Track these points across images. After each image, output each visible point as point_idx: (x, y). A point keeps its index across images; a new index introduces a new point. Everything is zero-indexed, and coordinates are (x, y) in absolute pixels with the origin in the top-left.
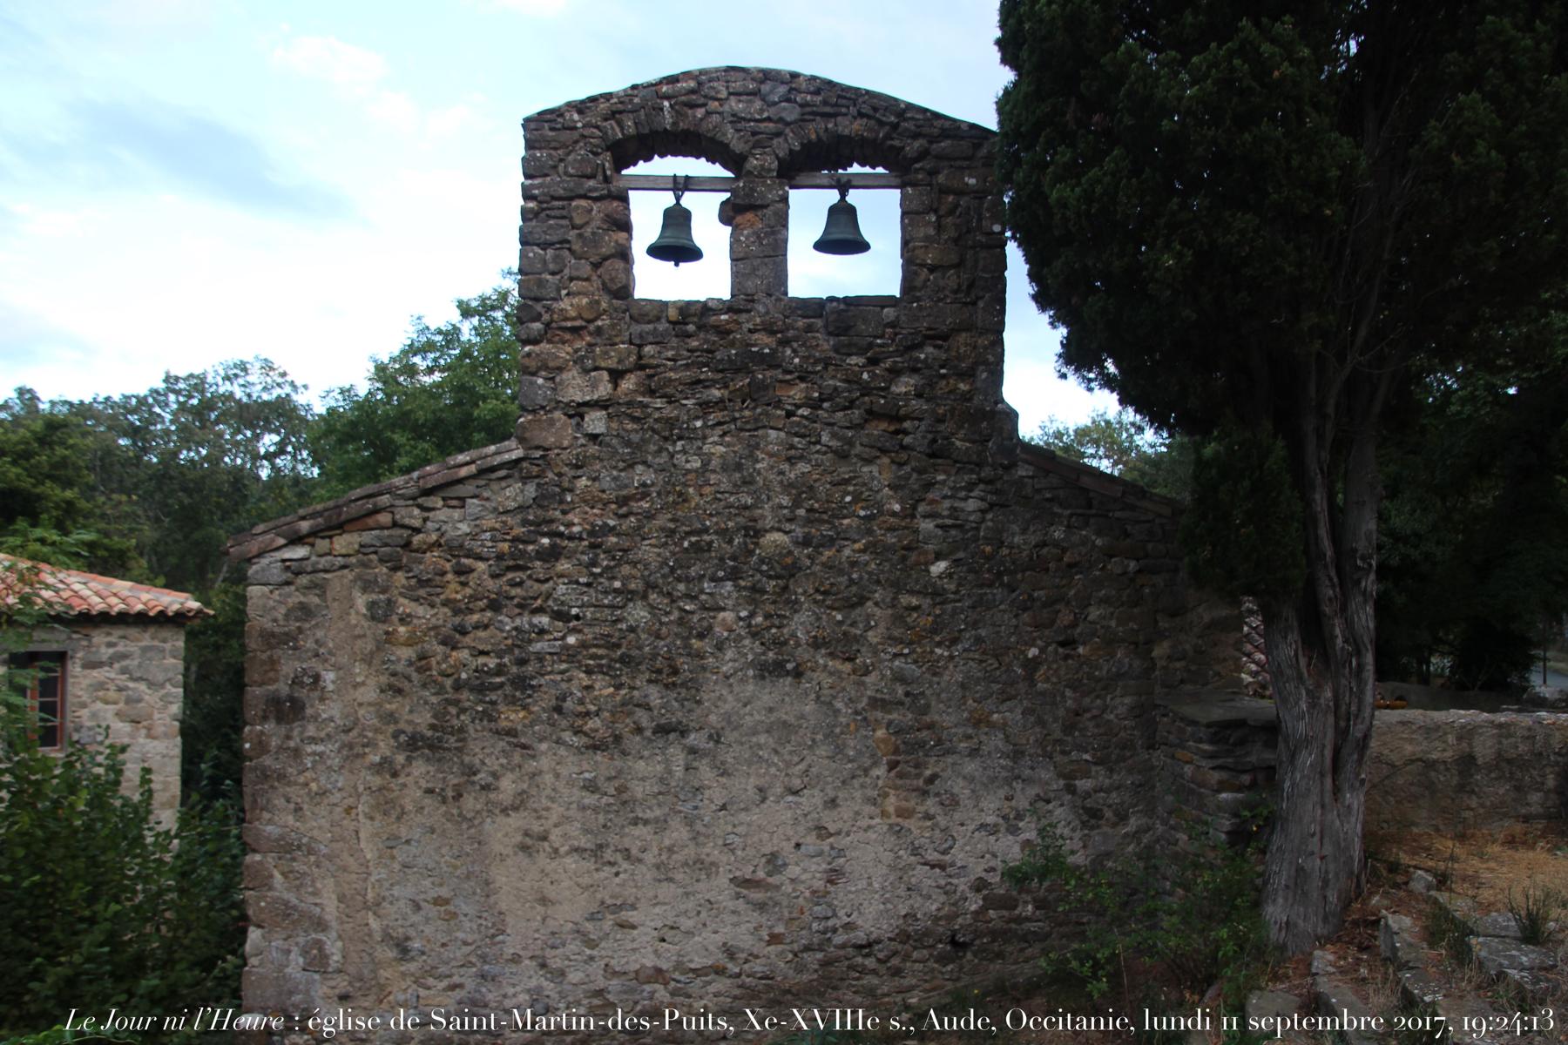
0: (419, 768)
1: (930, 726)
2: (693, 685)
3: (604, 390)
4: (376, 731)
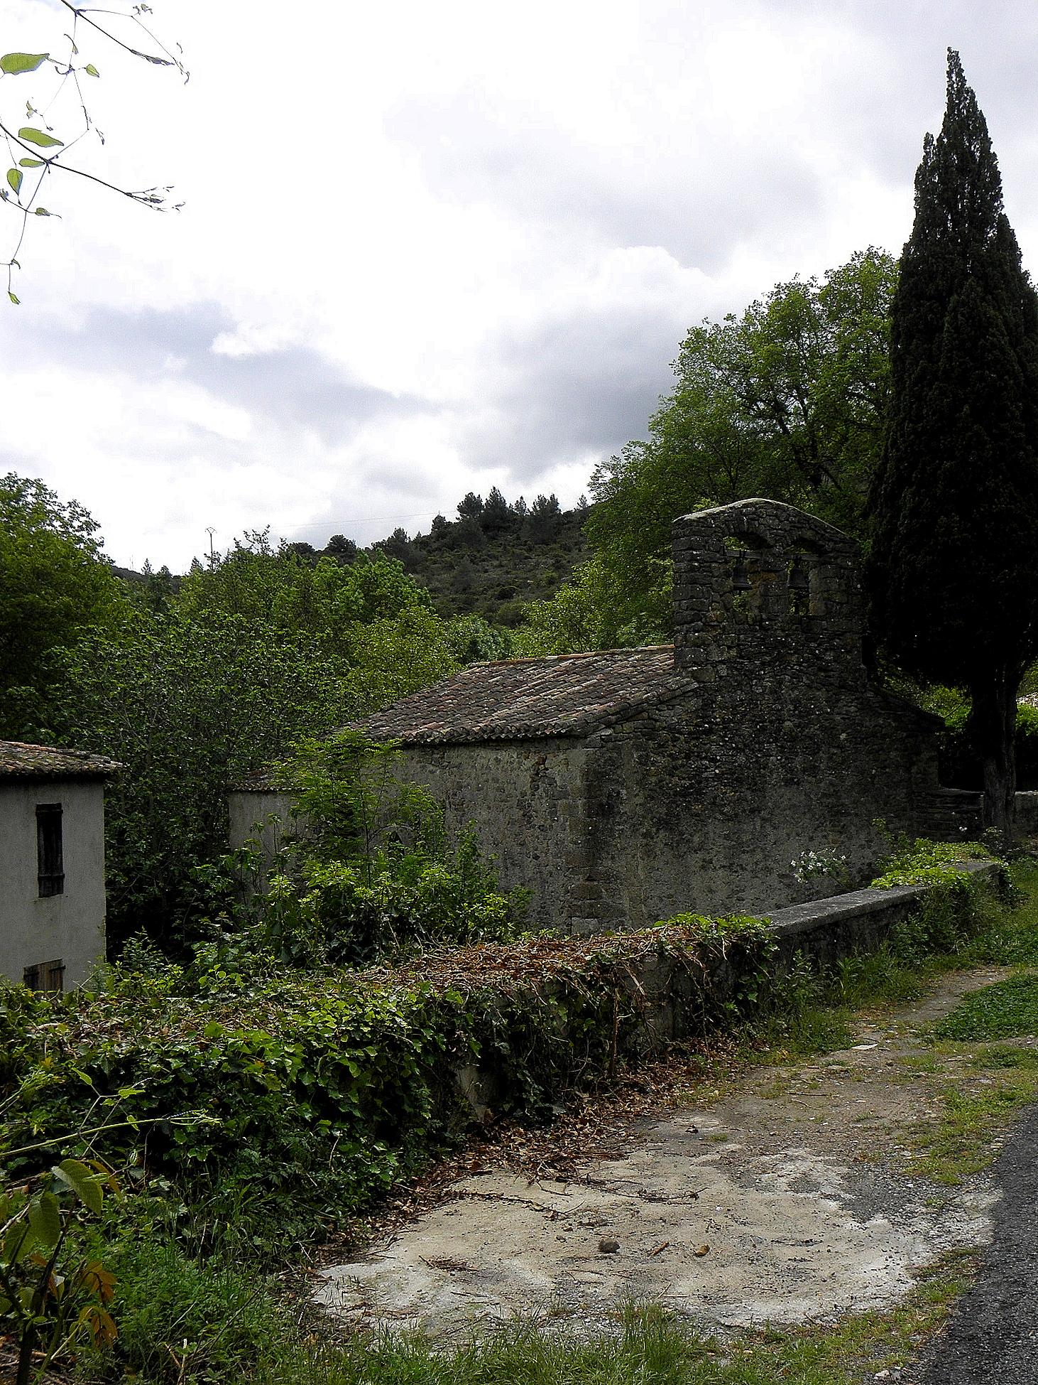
0: (662, 834)
1: (842, 804)
2: (763, 790)
3: (725, 656)
4: (644, 817)
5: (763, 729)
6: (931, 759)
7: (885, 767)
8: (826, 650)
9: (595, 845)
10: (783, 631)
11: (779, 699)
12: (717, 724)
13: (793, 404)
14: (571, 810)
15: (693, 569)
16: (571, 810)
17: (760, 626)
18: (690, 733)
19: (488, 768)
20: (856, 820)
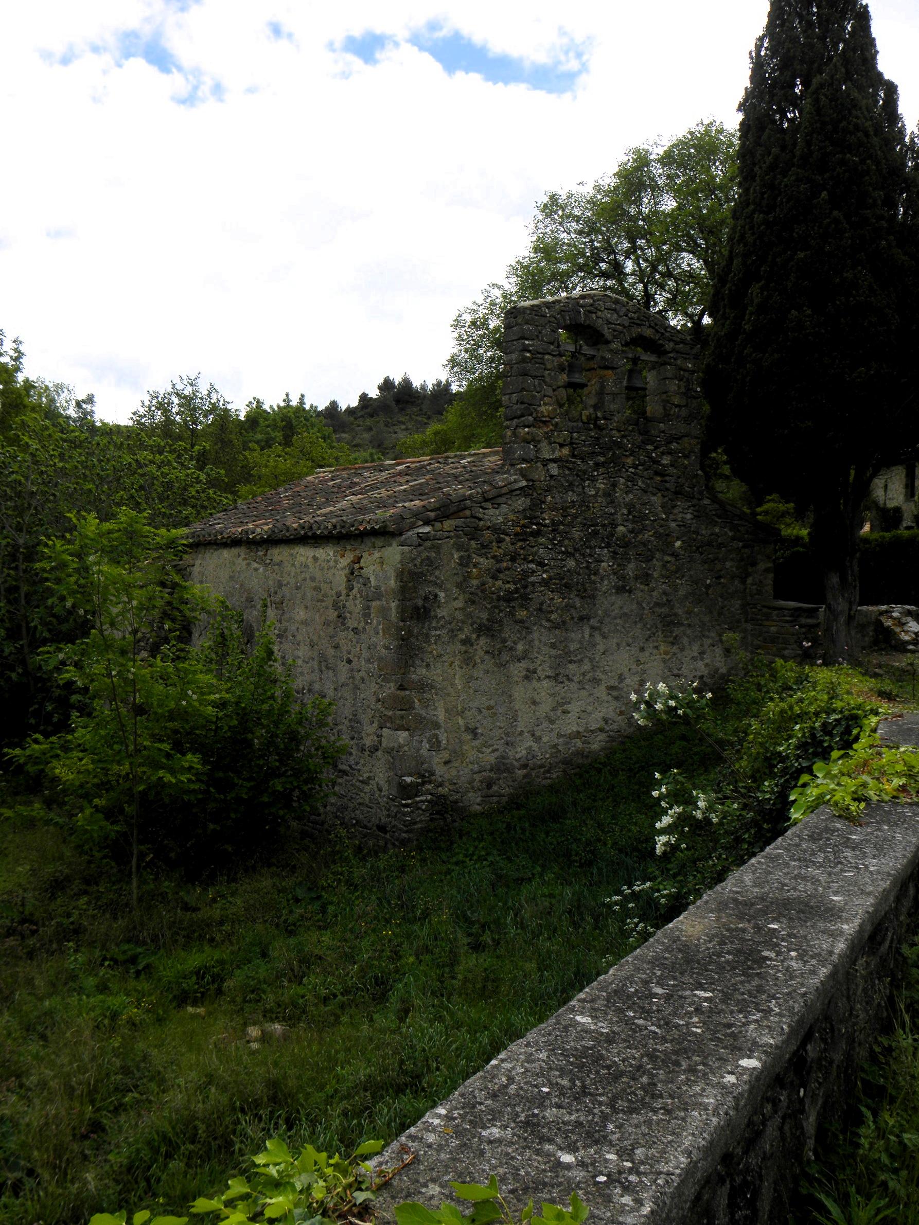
2: (593, 597)
3: (557, 454)
4: (463, 622)
5: (595, 533)
6: (767, 570)
7: (719, 578)
8: (663, 453)
9: (408, 650)
10: (619, 431)
11: (612, 502)
12: (545, 526)
13: (629, 266)
14: (384, 611)
15: (524, 360)
16: (384, 611)
17: (595, 425)
18: (516, 534)
19: (306, 566)
20: (689, 632)
